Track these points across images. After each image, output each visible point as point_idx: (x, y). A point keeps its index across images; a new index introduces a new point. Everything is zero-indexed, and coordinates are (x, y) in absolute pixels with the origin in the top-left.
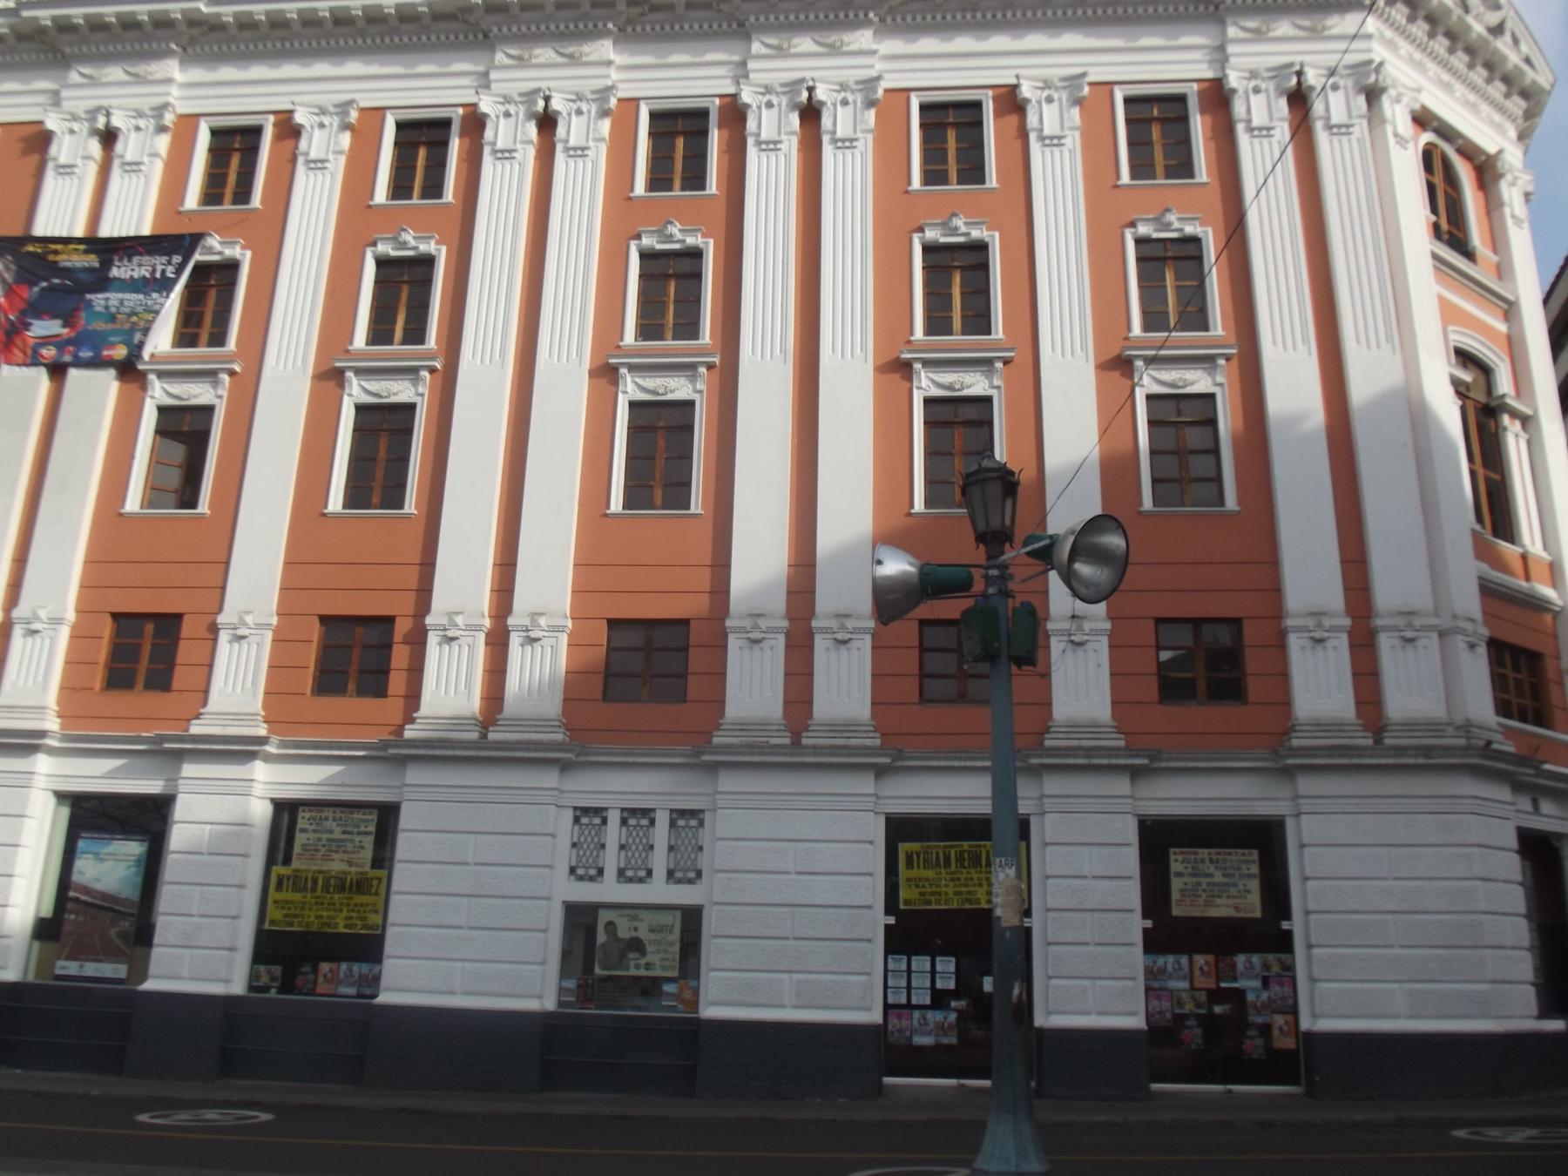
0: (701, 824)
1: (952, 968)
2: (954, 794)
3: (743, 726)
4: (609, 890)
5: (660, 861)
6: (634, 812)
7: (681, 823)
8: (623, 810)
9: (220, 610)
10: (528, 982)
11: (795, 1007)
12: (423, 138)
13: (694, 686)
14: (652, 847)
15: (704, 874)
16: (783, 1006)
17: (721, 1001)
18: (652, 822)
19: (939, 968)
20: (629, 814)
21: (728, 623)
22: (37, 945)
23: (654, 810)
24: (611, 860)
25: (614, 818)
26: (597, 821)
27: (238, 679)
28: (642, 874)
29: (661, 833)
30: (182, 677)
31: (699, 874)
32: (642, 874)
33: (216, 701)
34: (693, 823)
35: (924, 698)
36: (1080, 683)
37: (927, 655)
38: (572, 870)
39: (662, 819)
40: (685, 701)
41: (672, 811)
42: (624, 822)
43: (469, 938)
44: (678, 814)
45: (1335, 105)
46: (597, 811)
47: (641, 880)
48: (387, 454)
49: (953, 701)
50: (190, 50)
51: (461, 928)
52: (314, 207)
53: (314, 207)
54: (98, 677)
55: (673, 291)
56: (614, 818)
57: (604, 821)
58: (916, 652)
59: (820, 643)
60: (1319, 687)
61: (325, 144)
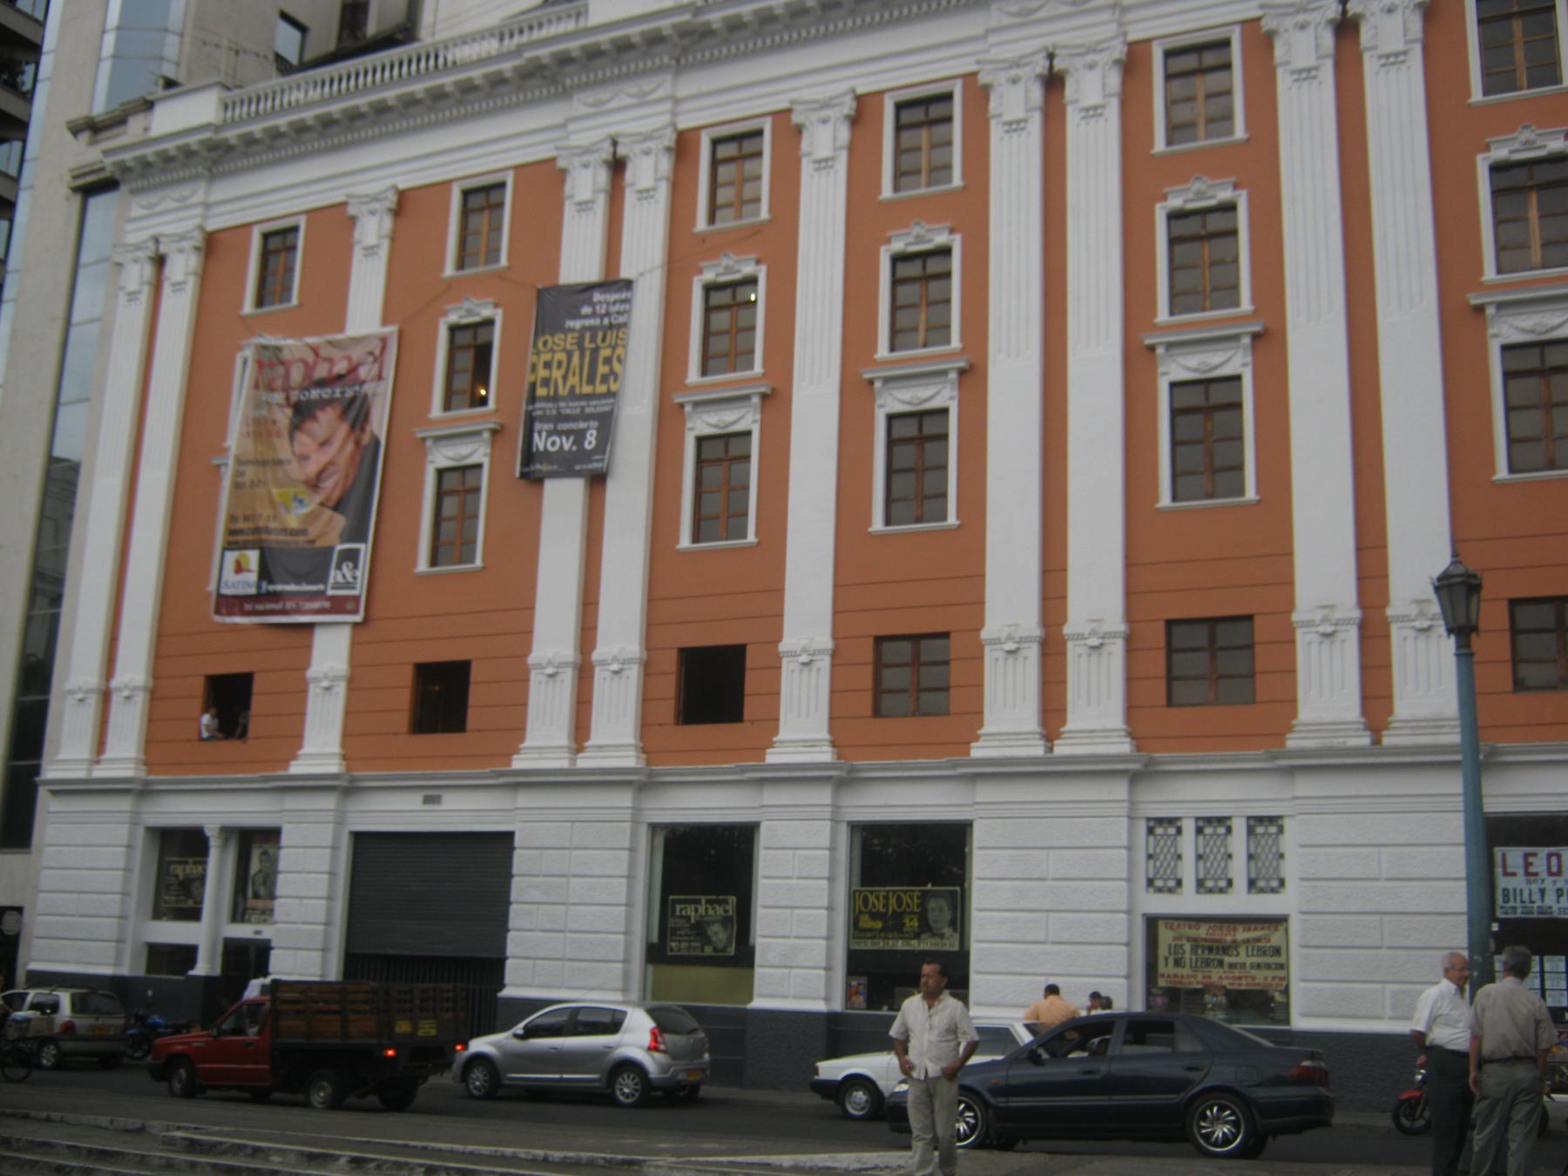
0: (1281, 830)
1: (1562, 967)
2: (1560, 791)
3: (1318, 727)
4: (1189, 902)
5: (1238, 870)
6: (1209, 820)
7: (1260, 830)
8: (1198, 819)
9: (779, 640)
10: (1109, 977)
11: (1392, 1018)
12: (923, 112)
13: (1263, 685)
14: (1230, 856)
15: (1287, 883)
16: (1380, 1018)
17: (1312, 1011)
18: (1229, 830)
19: (1547, 967)
20: (1203, 823)
21: (1295, 617)
22: (650, 968)
23: (1229, 818)
24: (1188, 871)
25: (1189, 827)
26: (1172, 831)
27: (802, 710)
28: (1222, 884)
29: (1238, 842)
30: (751, 706)
31: (1282, 883)
32: (1222, 884)
33: (1308, 710)
34: (1273, 829)
35: (1519, 685)
37: (1521, 637)
38: (1150, 882)
39: (1239, 827)
40: (1254, 702)
41: (1249, 818)
42: (1199, 831)
43: (1050, 934)
44: (1255, 822)
46: (1171, 821)
47: (1221, 891)
48: (917, 461)
49: (1553, 687)
50: (683, 61)
51: (1044, 943)
54: (667, 709)
55: (1201, 252)
56: (1189, 827)
57: (1179, 831)
58: (1506, 637)
59: (1073, 650)
61: (825, 140)
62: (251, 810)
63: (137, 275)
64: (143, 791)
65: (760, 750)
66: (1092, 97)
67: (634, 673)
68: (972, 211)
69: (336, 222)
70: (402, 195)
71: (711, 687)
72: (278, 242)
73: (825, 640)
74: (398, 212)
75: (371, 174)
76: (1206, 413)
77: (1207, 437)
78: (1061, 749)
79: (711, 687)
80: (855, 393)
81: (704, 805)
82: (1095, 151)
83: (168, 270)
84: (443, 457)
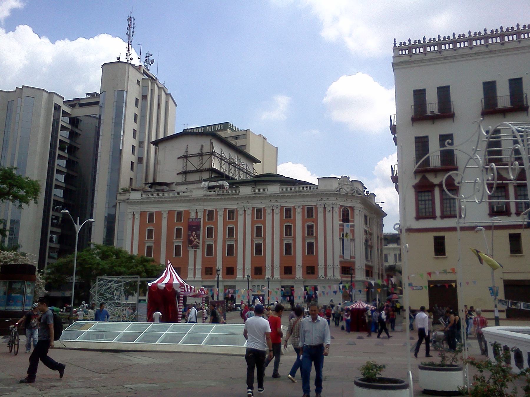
27: (299, 273)
36: (299, 273)
45: (328, 209)
48: (231, 249)
52: (220, 220)
53: (220, 220)
54: (225, 273)
55: (259, 231)
60: (321, 273)
61: (221, 213)
62: (314, 283)
63: (130, 216)
64: (202, 282)
65: (236, 278)
66: (249, 213)
67: (201, 270)
68: (236, 223)
69: (159, 213)
70: (169, 211)
71: (288, 270)
72: (151, 215)
73: (201, 267)
74: (168, 213)
75: (165, 208)
76: (230, 247)
77: (259, 249)
78: (195, 279)
79: (288, 270)
80: (224, 242)
81: (288, 283)
82: (277, 218)
83: (334, 209)
84: (147, 245)
